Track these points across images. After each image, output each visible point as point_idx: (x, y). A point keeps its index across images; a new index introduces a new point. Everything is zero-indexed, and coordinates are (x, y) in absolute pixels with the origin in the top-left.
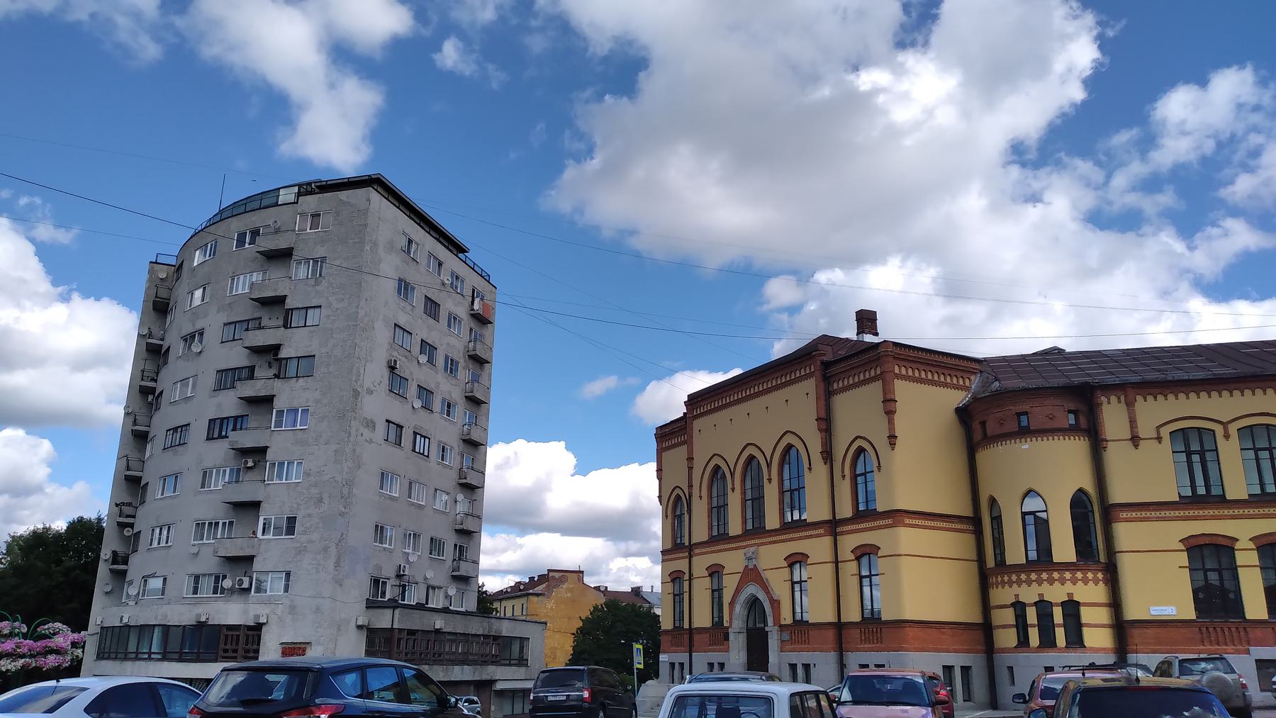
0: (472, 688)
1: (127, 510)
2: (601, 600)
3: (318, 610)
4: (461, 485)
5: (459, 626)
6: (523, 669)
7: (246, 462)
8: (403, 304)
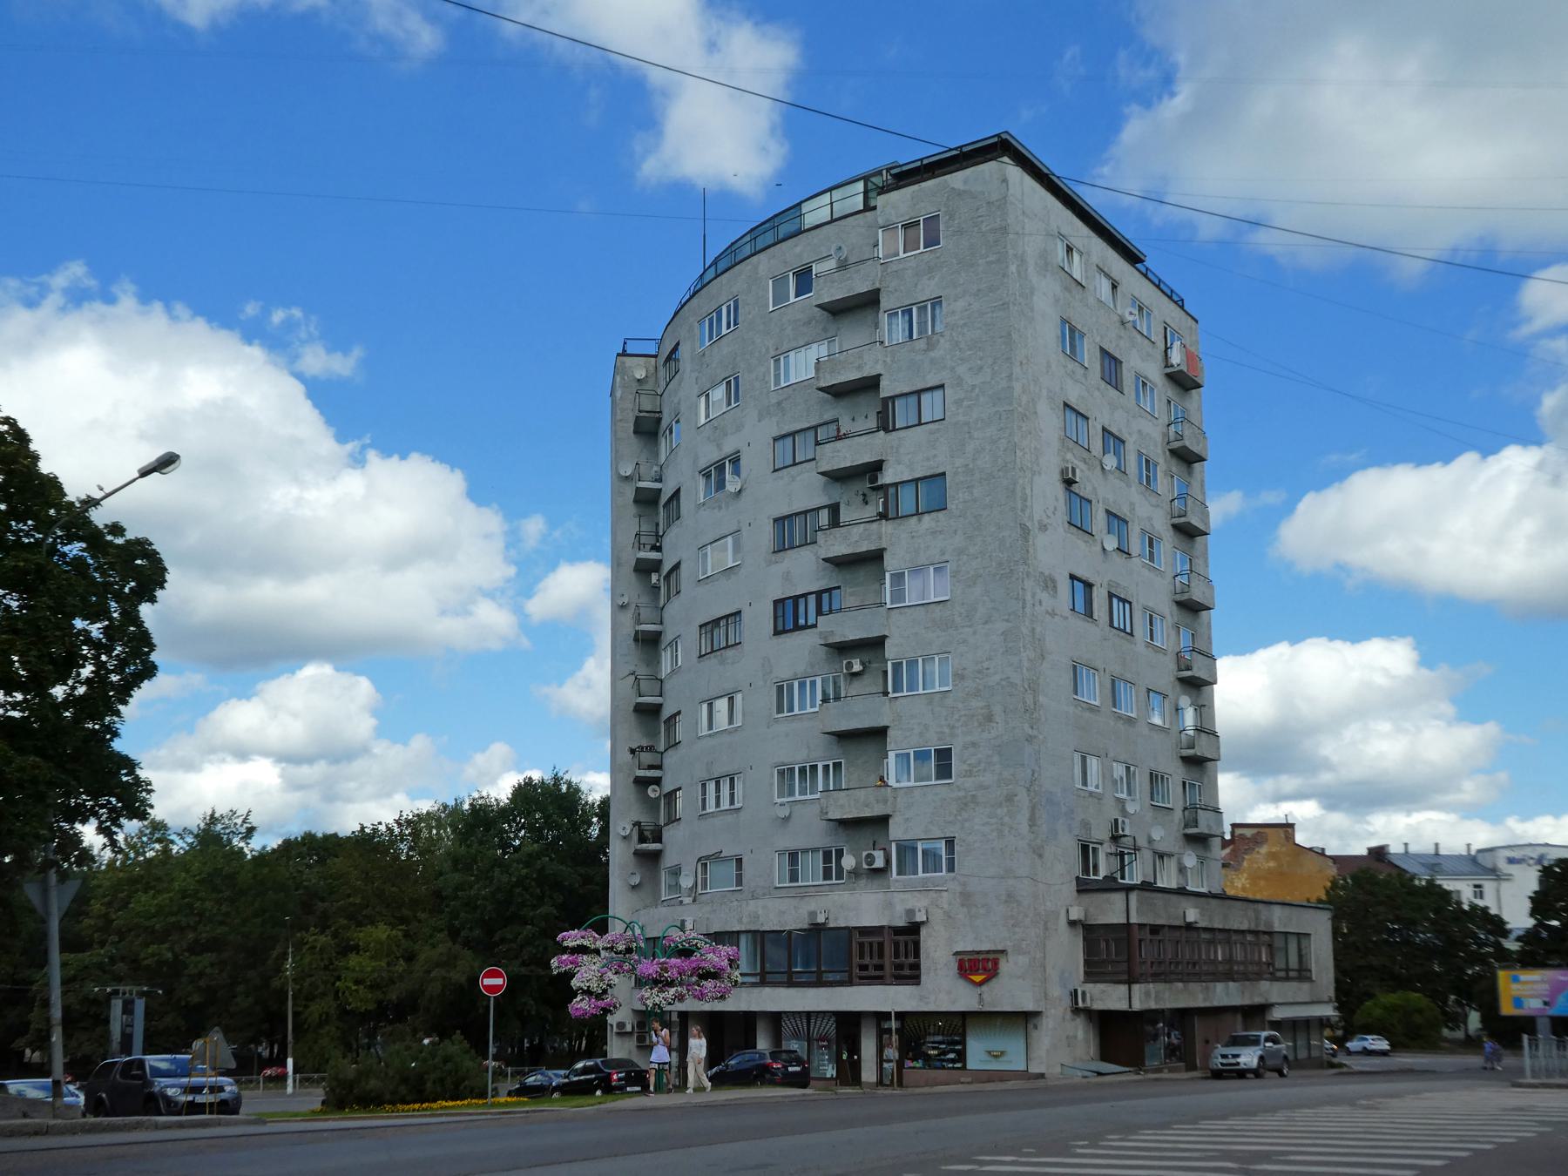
0: (1239, 1018)
1: (647, 758)
2: (1333, 871)
3: (1010, 897)
4: (1182, 680)
6: (1306, 986)
7: (850, 665)
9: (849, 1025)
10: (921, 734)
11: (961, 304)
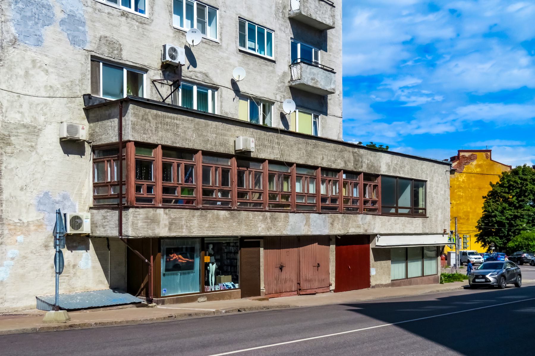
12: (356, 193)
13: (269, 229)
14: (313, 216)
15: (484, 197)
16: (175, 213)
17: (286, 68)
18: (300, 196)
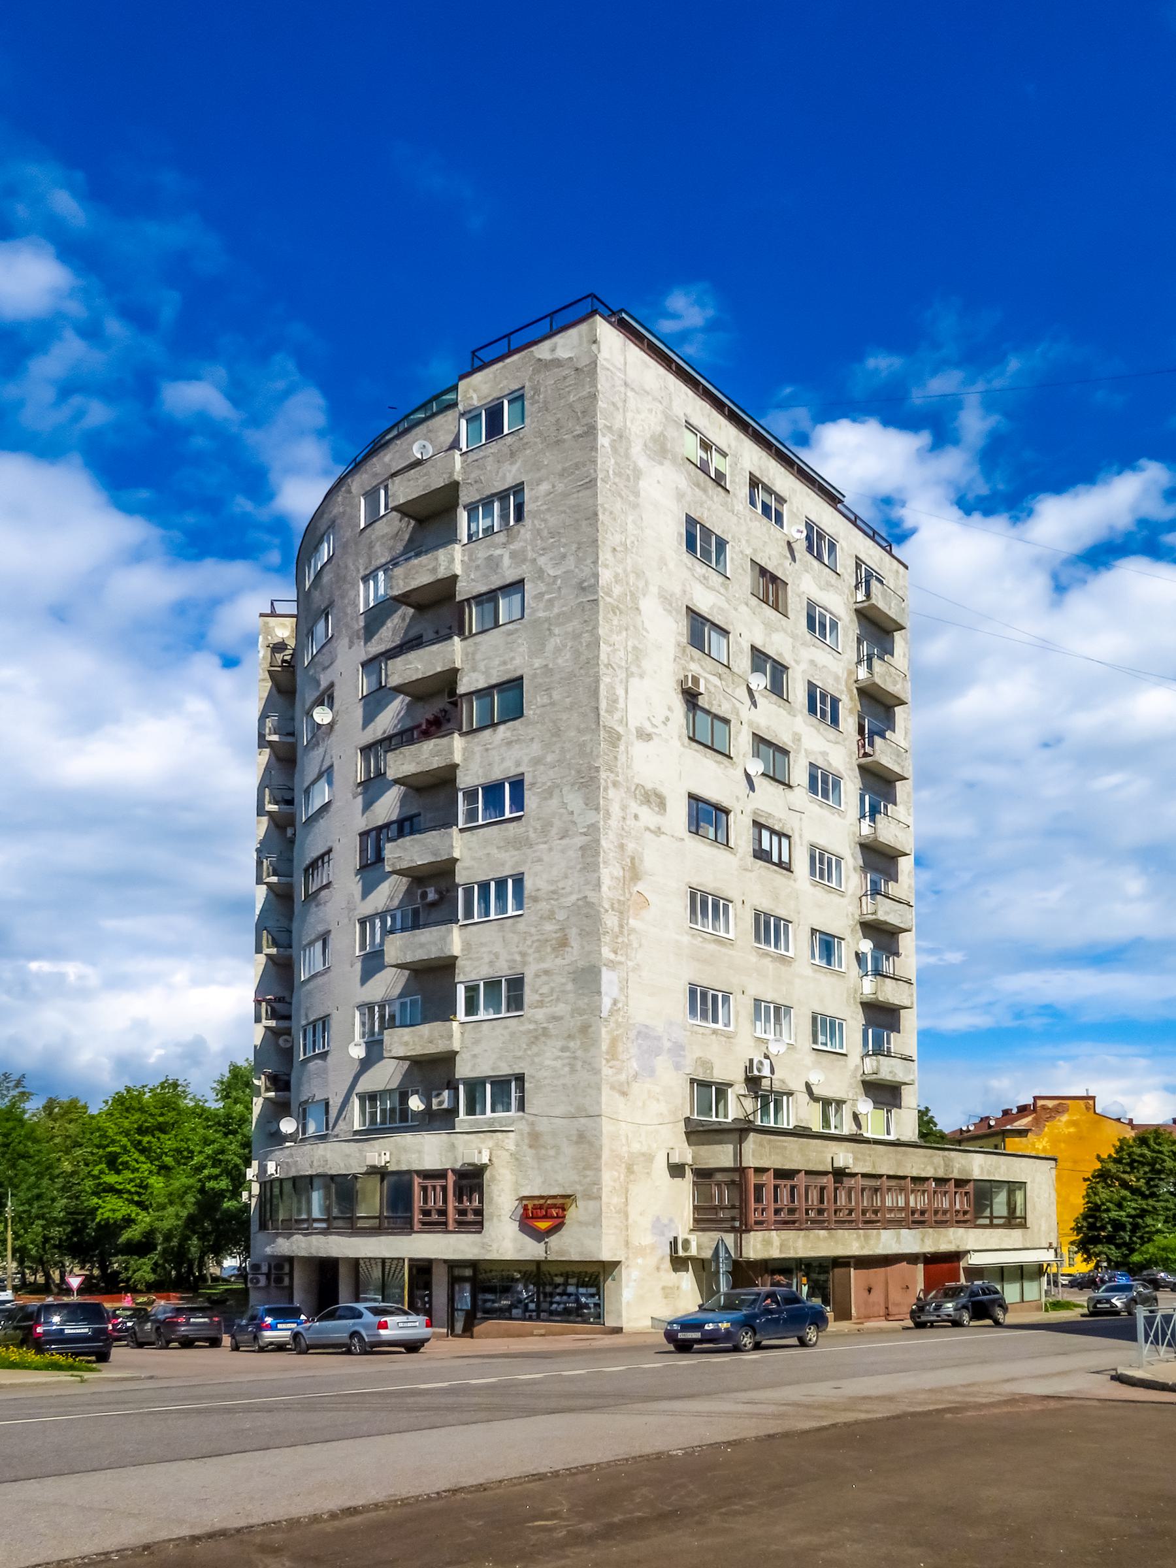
5: (885, 1163)
7: (424, 895)
8: (701, 569)
9: (422, 1270)
10: (491, 963)
11: (545, 487)
12: (946, 1205)
13: (862, 1248)
14: (904, 1232)
15: (1085, 1180)
16: (785, 1234)
17: (859, 1060)
18: (891, 1210)
